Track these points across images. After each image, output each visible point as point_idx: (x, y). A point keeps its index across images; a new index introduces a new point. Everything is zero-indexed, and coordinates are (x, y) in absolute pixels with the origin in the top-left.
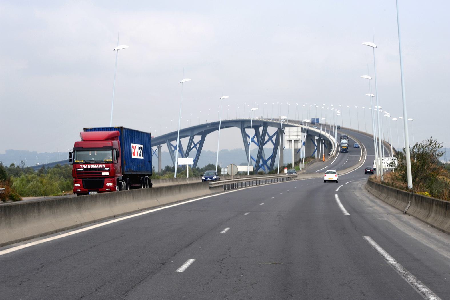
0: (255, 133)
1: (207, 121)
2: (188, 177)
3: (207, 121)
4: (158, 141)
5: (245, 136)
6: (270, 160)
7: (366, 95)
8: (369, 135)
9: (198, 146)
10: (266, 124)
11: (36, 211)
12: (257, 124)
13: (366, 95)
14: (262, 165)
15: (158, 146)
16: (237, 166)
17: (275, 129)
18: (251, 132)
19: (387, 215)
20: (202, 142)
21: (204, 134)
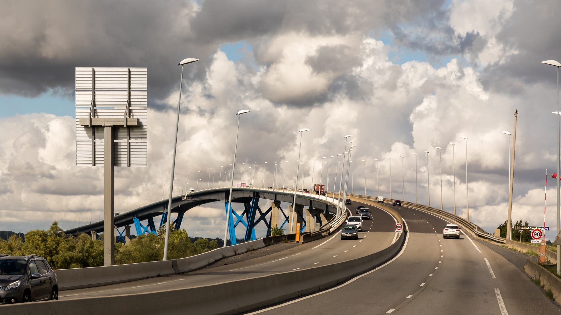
10: (257, 194)
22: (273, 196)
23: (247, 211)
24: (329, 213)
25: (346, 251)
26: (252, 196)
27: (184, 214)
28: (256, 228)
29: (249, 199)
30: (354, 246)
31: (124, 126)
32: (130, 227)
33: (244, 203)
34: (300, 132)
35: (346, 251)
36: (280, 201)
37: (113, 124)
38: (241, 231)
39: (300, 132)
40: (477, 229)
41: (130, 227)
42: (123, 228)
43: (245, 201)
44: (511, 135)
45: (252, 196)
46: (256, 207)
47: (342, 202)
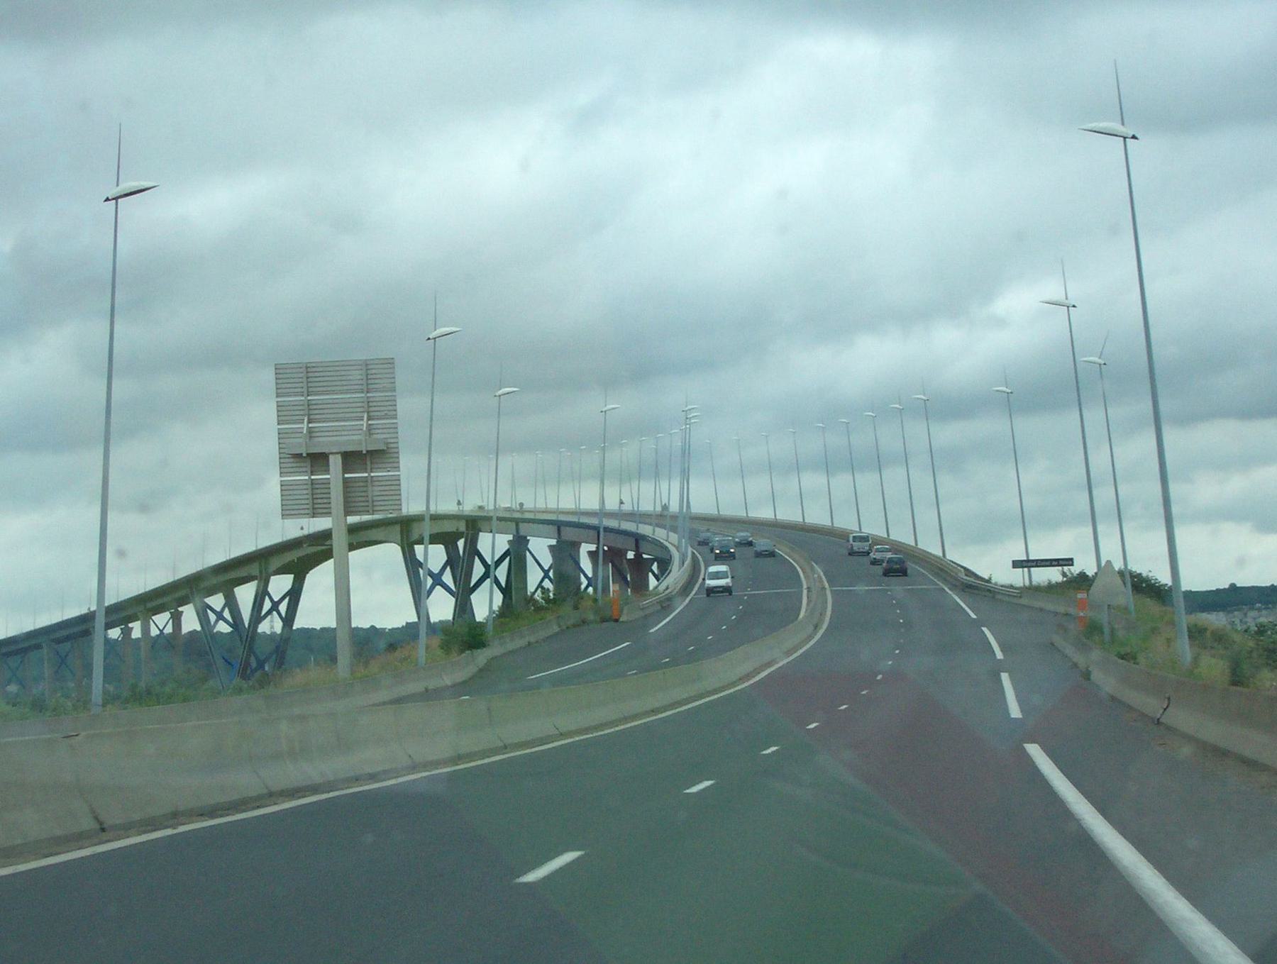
0: (445, 558)
1: (302, 528)
2: (999, 655)
3: (302, 528)
4: (124, 614)
5: (413, 565)
6: (287, 600)
7: (984, 629)
8: (359, 451)
9: (283, 608)
10: (474, 524)
11: (288, 763)
12: (448, 527)
13: (984, 629)
14: (269, 612)
15: (121, 629)
16: (231, 629)
17: (503, 542)
18: (435, 556)
19: (1116, 658)
20: (294, 595)
21: (300, 571)
22: (513, 525)
23: (451, 562)
24: (642, 557)
25: (845, 707)
26: (462, 528)
27: (308, 575)
28: (474, 598)
29: (457, 536)
30: (710, 638)
31: (362, 451)
32: (182, 612)
33: (443, 544)
34: (429, 339)
35: (845, 707)
36: (526, 537)
37: (343, 449)
38: (441, 607)
39: (429, 339)
40: (964, 574)
41: (182, 612)
42: (167, 615)
43: (447, 540)
44: (1105, 364)
45: (462, 528)
46: (473, 552)
47: (675, 532)
